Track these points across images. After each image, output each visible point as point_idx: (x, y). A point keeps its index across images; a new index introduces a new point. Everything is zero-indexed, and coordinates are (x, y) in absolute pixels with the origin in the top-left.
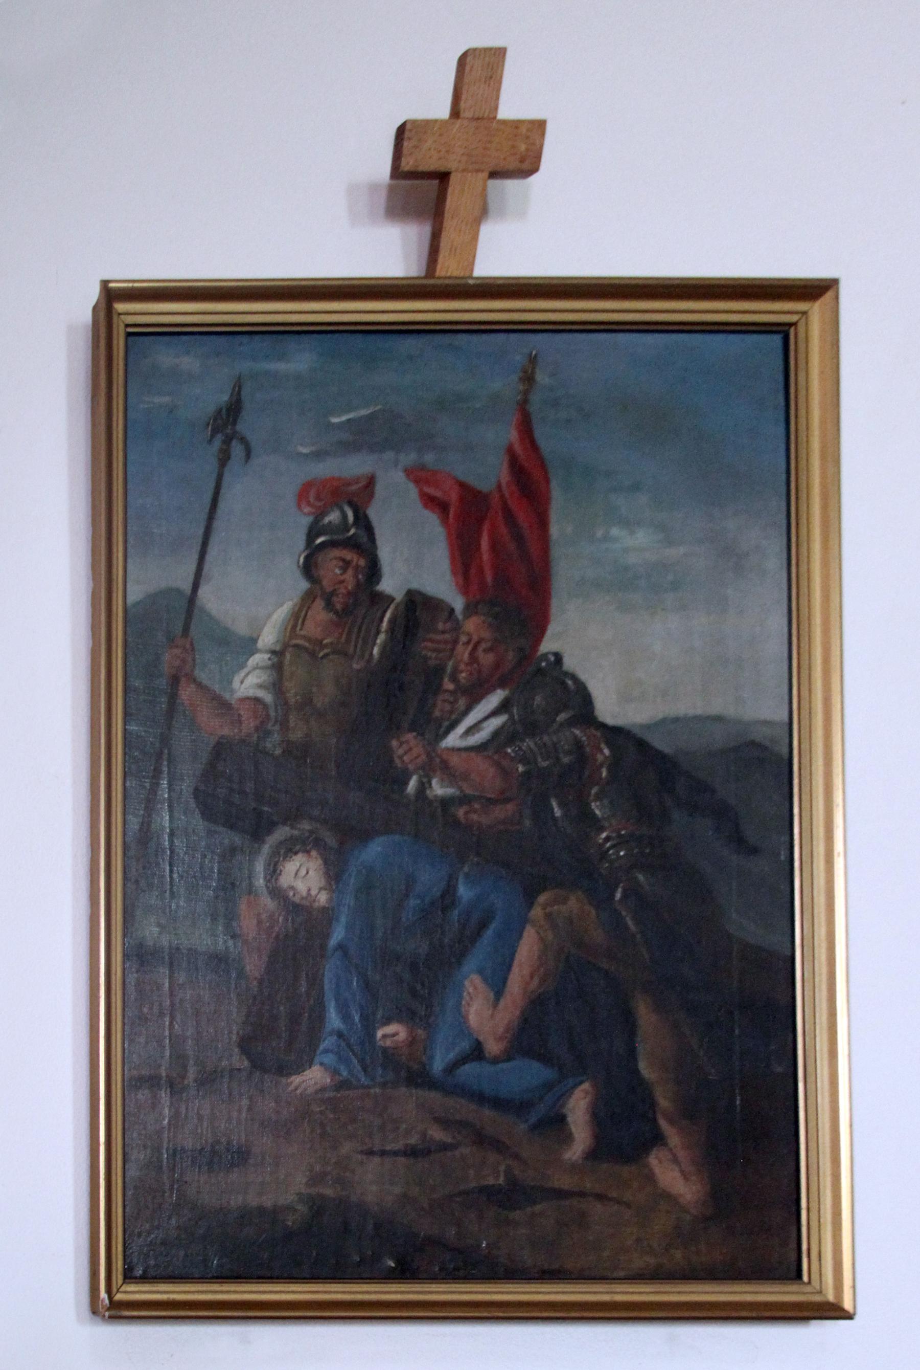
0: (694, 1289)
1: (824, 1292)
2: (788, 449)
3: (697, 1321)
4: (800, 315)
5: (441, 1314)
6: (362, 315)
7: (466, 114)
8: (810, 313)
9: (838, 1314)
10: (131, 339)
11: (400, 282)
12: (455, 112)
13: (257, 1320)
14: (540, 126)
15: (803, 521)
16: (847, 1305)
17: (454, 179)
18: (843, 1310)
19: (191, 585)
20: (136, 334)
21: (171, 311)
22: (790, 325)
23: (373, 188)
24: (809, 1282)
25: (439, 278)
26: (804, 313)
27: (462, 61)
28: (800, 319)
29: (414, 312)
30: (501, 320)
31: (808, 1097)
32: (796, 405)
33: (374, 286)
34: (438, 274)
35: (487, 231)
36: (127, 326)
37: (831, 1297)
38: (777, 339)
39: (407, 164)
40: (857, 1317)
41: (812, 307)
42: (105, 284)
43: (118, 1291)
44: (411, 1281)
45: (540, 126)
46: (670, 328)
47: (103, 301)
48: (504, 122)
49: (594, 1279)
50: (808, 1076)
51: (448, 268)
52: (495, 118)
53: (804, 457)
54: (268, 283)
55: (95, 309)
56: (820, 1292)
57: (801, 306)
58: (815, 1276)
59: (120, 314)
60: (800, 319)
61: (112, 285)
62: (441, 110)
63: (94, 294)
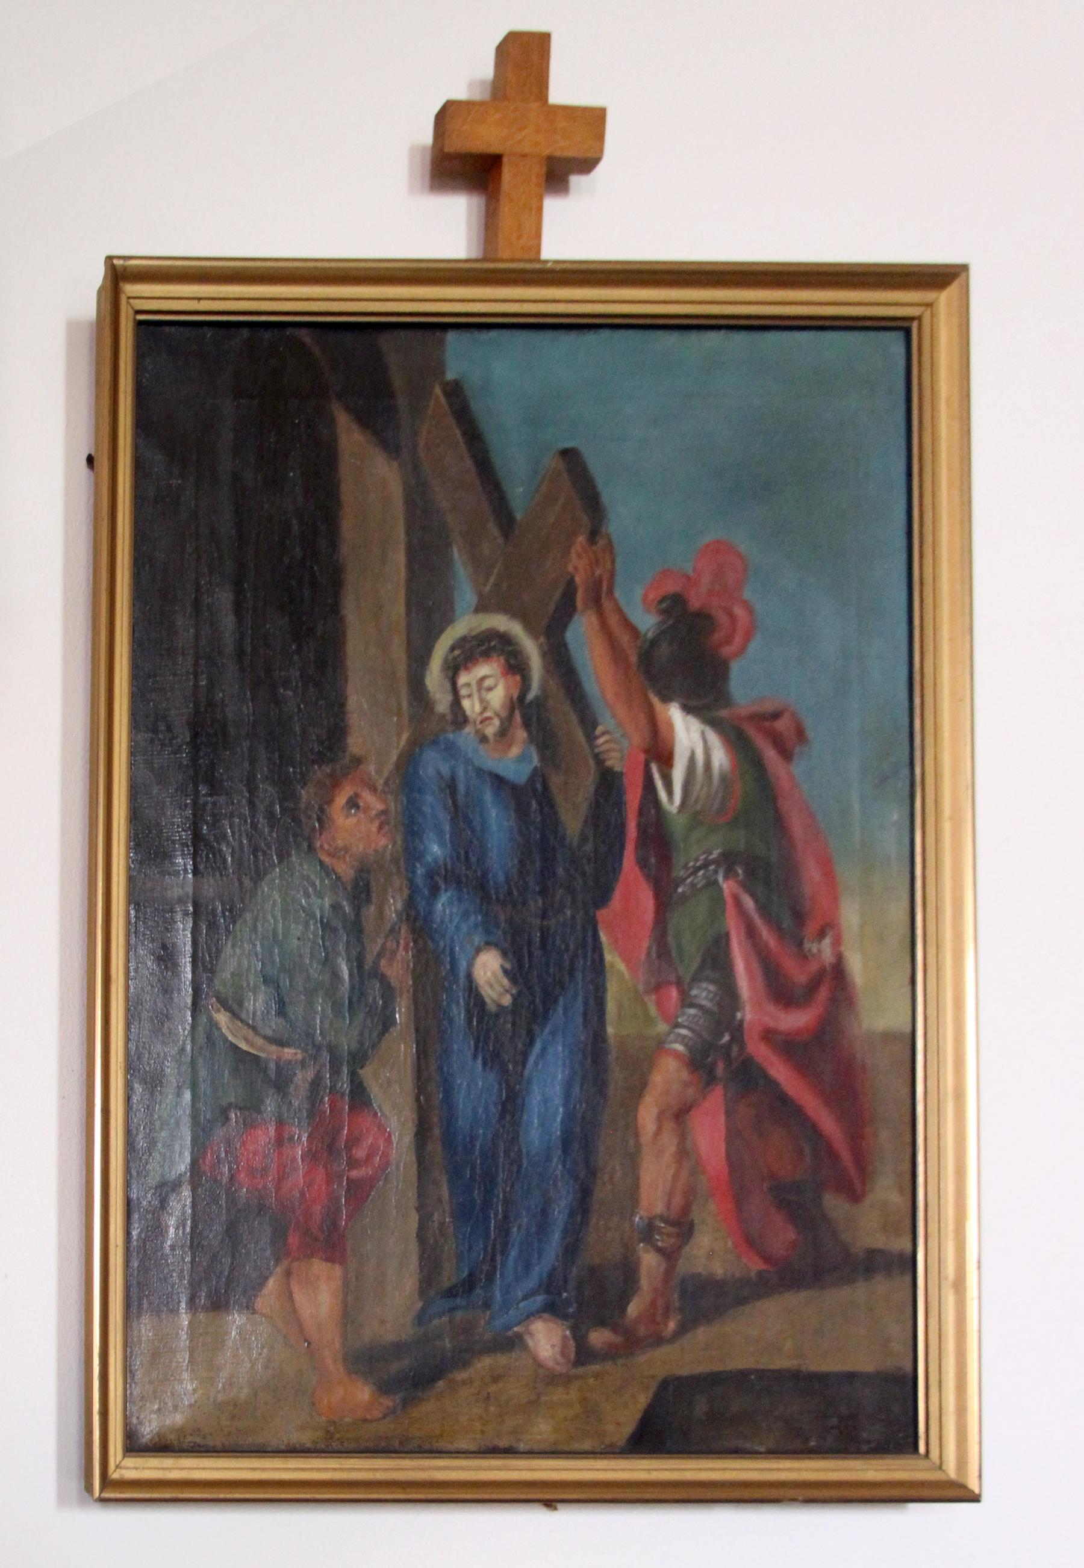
1: (944, 1467)
2: (909, 474)
6: (262, 303)
11: (461, 265)
15: (928, 468)
16: (973, 1485)
21: (415, 297)
22: (911, 319)
23: (424, 148)
26: (929, 305)
31: (927, 967)
32: (921, 505)
36: (138, 312)
40: (985, 1498)
42: (109, 259)
50: (929, 1221)
53: (931, 648)
55: (99, 292)
56: (940, 1467)
57: (928, 296)
59: (129, 298)
61: (115, 262)
63: (97, 275)
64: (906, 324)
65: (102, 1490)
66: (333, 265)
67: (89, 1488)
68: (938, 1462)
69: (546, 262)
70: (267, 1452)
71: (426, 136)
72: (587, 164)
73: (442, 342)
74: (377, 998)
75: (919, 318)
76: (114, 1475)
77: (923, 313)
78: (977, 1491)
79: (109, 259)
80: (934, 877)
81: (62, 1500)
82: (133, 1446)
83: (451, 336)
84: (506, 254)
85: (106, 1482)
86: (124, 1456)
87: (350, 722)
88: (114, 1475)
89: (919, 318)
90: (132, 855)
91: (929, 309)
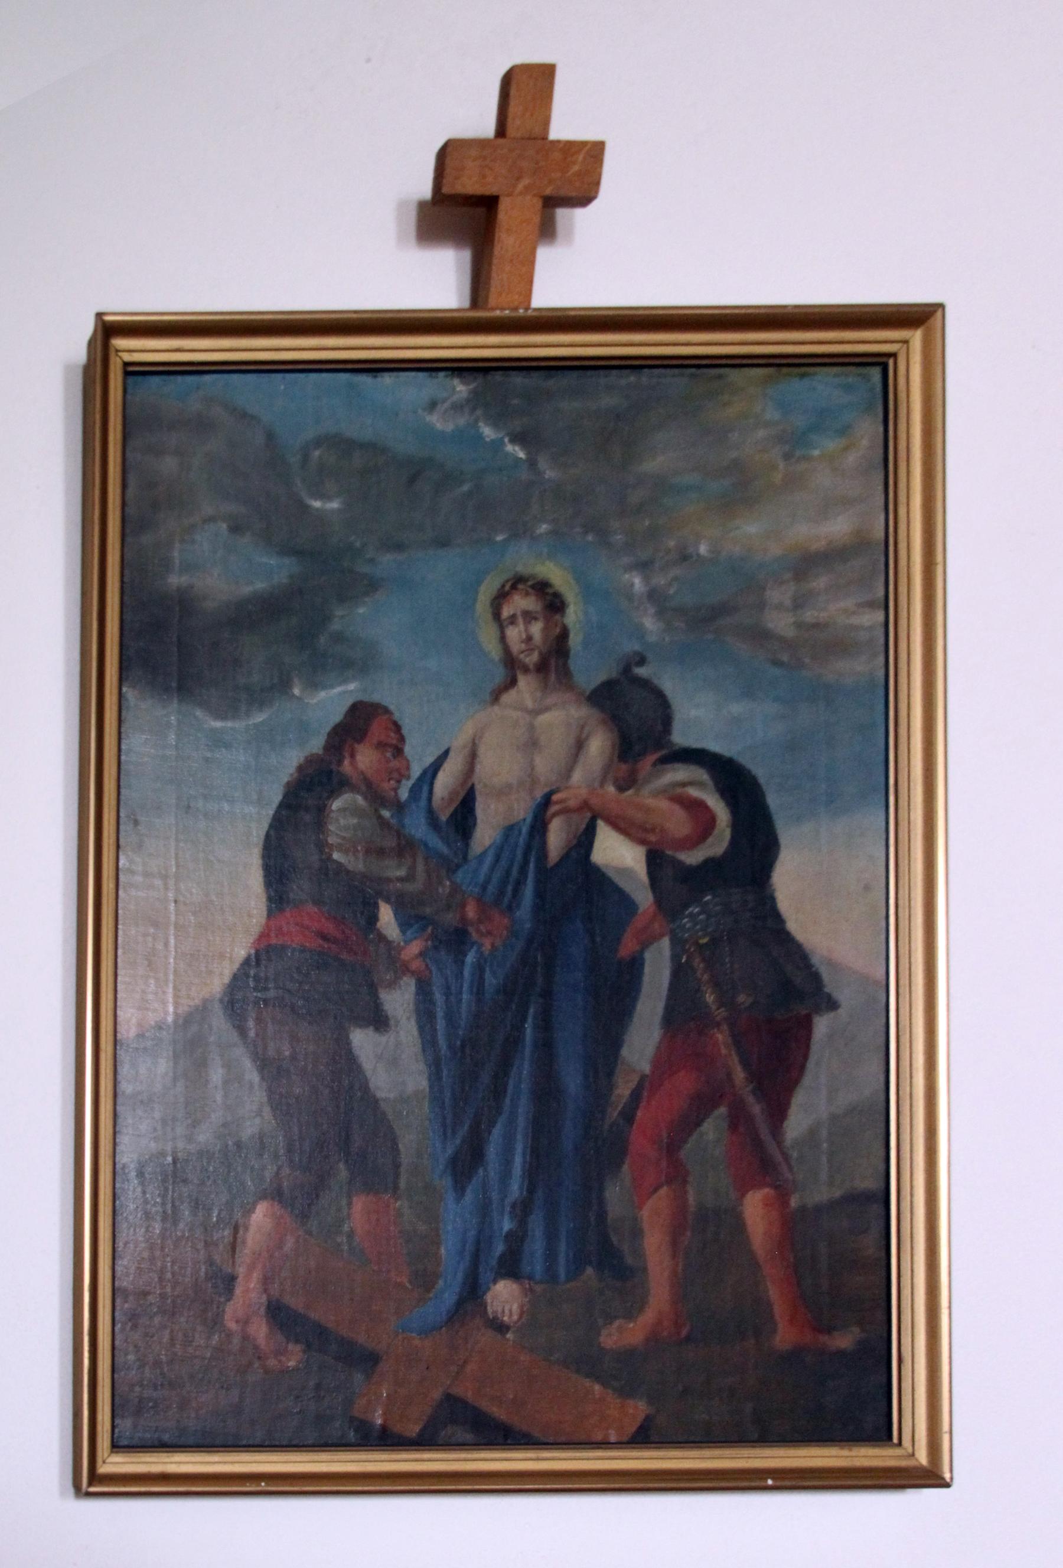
0: (143, 1460)
3: (438, 1494)
4: (900, 345)
5: (366, 1488)
7: (511, 131)
10: (131, 380)
12: (501, 130)
14: (595, 151)
17: (504, 205)
18: (943, 1479)
19: (509, 644)
20: (133, 371)
24: (900, 1444)
26: (906, 342)
27: (508, 81)
28: (901, 348)
30: (530, 356)
33: (775, 315)
35: (545, 256)
36: (126, 364)
37: (922, 1457)
38: (875, 373)
39: (445, 190)
41: (913, 336)
42: (99, 315)
43: (104, 1462)
45: (595, 151)
46: (755, 361)
47: (99, 337)
48: (553, 142)
49: (185, 1447)
55: (91, 343)
56: (913, 1455)
60: (901, 348)
61: (939, 313)
62: (486, 127)
63: (87, 328)
65: (90, 1484)
68: (910, 1450)
70: (240, 1447)
72: (585, 199)
74: (450, 978)
75: (894, 355)
76: (103, 1469)
77: (899, 350)
78: (948, 1480)
79: (99, 315)
85: (95, 1477)
88: (103, 1469)
91: (905, 345)
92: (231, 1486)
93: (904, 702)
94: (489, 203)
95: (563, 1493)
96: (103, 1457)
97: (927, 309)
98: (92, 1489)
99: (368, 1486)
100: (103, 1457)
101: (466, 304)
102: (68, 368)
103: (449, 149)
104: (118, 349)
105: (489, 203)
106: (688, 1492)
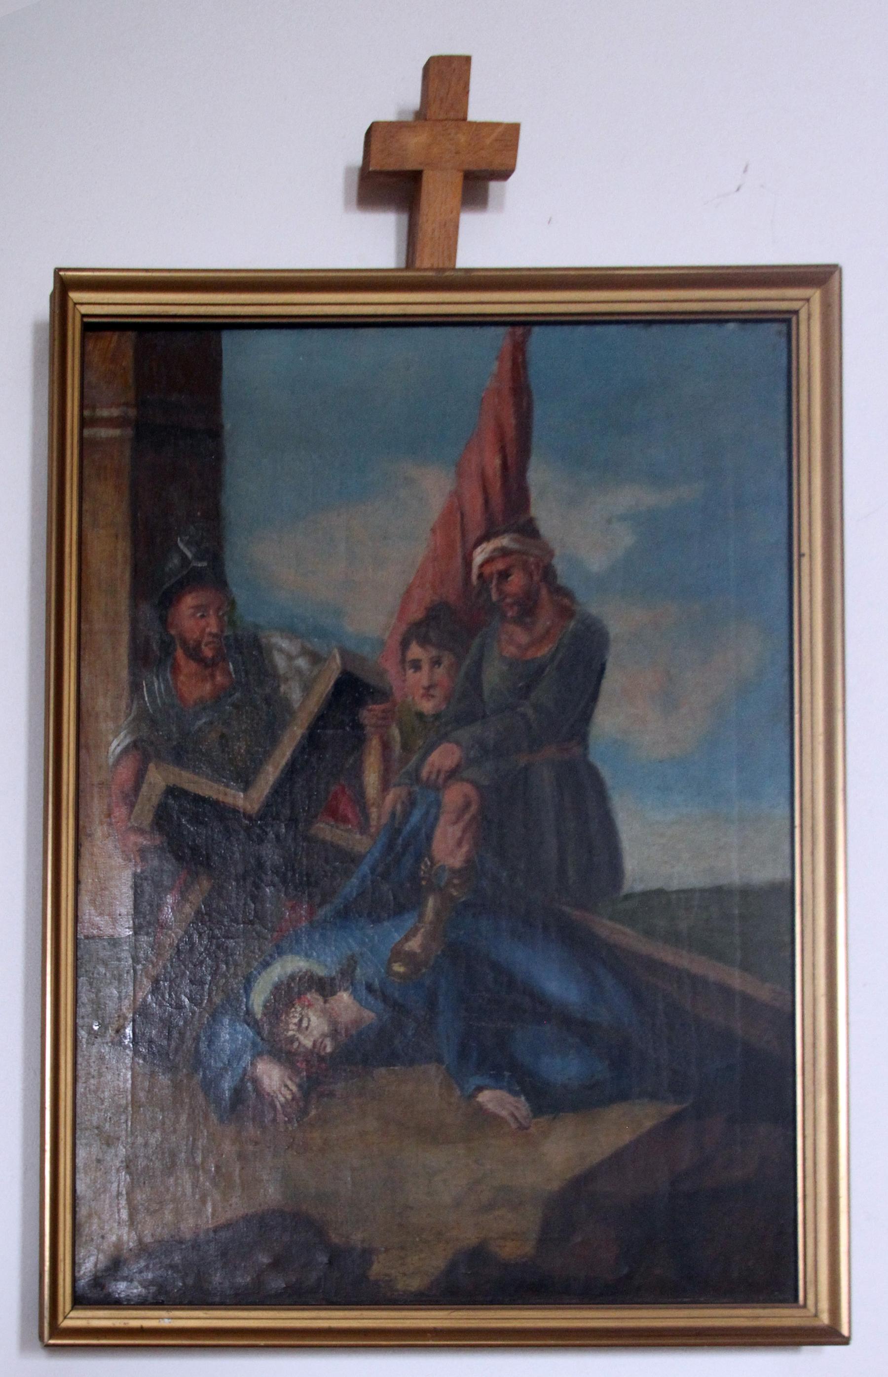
8: (812, 299)
9: (837, 1340)
13: (270, 1349)
16: (845, 1331)
18: (840, 1335)
24: (805, 1306)
25: (419, 270)
26: (808, 300)
27: (427, 69)
29: (438, 303)
34: (418, 264)
36: (83, 316)
37: (825, 1319)
42: (57, 271)
43: (65, 1318)
44: (107, 1307)
48: (472, 124)
51: (427, 260)
52: (465, 119)
54: (347, 274)
58: (811, 1297)
59: (75, 304)
61: (62, 273)
63: (48, 286)
64: (787, 316)
66: (380, 274)
67: (41, 1337)
69: (460, 270)
71: (357, 158)
72: (505, 174)
73: (529, 332)
75: (796, 312)
79: (57, 271)
80: (810, 761)
81: (24, 1345)
82: (79, 1301)
83: (536, 330)
84: (426, 264)
85: (56, 1331)
86: (73, 1309)
87: (406, 629)
89: (796, 312)
90: (234, 734)
92: (323, 1341)
93: (284, 755)
94: (416, 177)
95: (778, 1348)
96: (64, 1312)
97: (828, 269)
98: (52, 1342)
99: (395, 1340)
100: (64, 1312)
101: (403, 265)
102: (348, 170)
103: (373, 129)
104: (75, 301)
105: (416, 177)
106: (715, 1347)
